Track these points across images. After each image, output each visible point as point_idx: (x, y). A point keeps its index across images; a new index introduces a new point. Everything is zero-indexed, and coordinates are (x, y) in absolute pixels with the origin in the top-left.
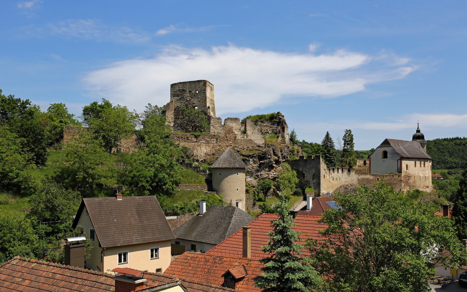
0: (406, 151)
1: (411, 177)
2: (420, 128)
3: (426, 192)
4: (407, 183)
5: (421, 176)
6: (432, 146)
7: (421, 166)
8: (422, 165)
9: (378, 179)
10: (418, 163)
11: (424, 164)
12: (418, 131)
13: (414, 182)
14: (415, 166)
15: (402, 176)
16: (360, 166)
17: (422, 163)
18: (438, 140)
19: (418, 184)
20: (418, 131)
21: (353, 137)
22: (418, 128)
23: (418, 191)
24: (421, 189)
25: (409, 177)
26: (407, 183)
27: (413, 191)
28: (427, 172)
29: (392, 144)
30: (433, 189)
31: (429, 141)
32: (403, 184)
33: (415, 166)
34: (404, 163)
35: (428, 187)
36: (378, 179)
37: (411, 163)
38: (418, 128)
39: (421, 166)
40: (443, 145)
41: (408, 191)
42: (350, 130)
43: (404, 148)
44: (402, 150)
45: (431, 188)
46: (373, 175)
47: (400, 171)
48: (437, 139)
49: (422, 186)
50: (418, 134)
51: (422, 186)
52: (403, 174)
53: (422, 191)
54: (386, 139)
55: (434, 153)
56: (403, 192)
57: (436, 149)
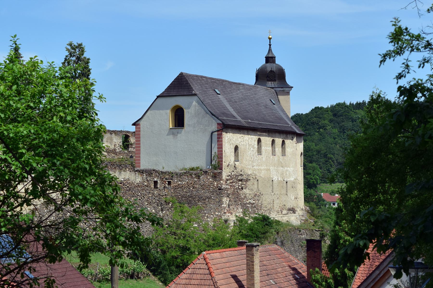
0: (235, 109)
1: (247, 180)
2: (275, 52)
3: (288, 224)
4: (237, 199)
5: (275, 178)
6: (326, 122)
7: (274, 153)
8: (278, 149)
9: (156, 183)
10: (266, 140)
11: (283, 143)
12: (270, 59)
13: (257, 196)
14: (259, 151)
15: (224, 175)
16: (114, 151)
17: (279, 141)
18: (339, 103)
19: (266, 200)
20: (270, 59)
21: (91, 66)
22: (270, 50)
23: (265, 221)
24: (274, 216)
25: (241, 179)
26: (237, 199)
27: (255, 219)
28: (291, 169)
29: (196, 89)
30: (307, 216)
31: (322, 108)
32: (226, 200)
33: (259, 151)
34: (230, 139)
35: (293, 210)
36: (156, 183)
37: (247, 141)
38: (270, 50)
39: (274, 153)
40: (353, 120)
41: (241, 220)
42: (80, 45)
43: (229, 101)
44: (225, 107)
45: (301, 213)
46: (141, 172)
47: (217, 166)
48: (338, 105)
49: (277, 207)
50: (270, 67)
51: (277, 207)
52: (225, 174)
53: (278, 222)
54: (181, 75)
55: (331, 140)
56: (226, 221)
57: (336, 131)
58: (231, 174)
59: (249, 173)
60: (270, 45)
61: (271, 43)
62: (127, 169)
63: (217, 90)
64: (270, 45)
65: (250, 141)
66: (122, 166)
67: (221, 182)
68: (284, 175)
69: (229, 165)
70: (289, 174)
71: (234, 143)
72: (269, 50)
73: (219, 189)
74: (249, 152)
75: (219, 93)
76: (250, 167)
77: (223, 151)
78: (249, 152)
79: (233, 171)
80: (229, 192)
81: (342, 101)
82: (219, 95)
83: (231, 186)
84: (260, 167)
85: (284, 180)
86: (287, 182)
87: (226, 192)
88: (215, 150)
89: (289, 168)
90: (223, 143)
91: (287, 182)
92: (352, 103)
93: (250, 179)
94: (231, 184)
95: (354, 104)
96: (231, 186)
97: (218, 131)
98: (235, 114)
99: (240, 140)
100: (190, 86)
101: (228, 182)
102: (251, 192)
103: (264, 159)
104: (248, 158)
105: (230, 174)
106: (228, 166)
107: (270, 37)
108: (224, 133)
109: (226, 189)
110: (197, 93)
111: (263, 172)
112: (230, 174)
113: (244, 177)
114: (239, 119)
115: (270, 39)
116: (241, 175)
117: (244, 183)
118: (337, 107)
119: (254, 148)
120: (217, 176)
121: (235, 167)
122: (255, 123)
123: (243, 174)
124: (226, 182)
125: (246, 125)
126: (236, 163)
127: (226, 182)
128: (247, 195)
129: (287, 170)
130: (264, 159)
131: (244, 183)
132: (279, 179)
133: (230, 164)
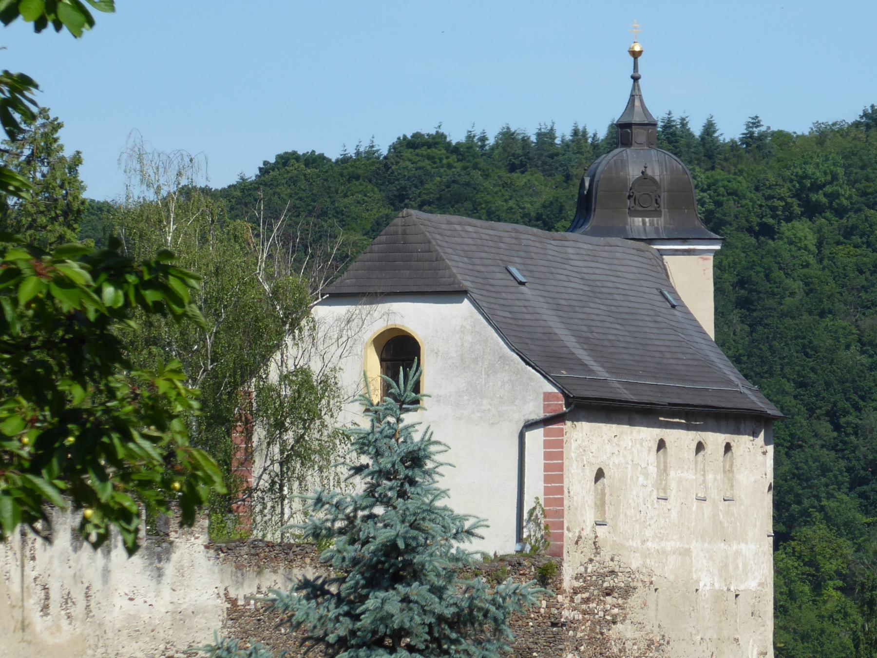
31: (314, 160)
48: (413, 144)
58: (586, 568)
59: (634, 567)
60: (636, 79)
61: (641, 72)
62: (308, 560)
63: (514, 270)
64: (636, 79)
65: (635, 451)
66: (294, 549)
67: (560, 598)
68: (731, 568)
69: (580, 537)
70: (745, 565)
71: (593, 460)
72: (632, 97)
73: (554, 625)
74: (634, 493)
75: (523, 280)
76: (635, 544)
77: (566, 491)
78: (634, 493)
79: (591, 560)
80: (579, 635)
81: (428, 129)
82: (523, 288)
83: (584, 613)
84: (663, 544)
85: (729, 590)
86: (737, 596)
87: (571, 633)
88: (535, 489)
89: (743, 546)
90: (566, 463)
91: (737, 596)
92: (478, 133)
93: (635, 588)
94: (584, 607)
95: (491, 141)
96: (584, 613)
97: (546, 422)
98: (581, 354)
99: (609, 448)
100: (439, 259)
101: (578, 598)
102: (637, 635)
103: (674, 514)
104: (631, 512)
105: (582, 569)
106: (577, 543)
107: (637, 48)
108: (754, 461)
109: (571, 624)
110: (467, 285)
111: (672, 559)
112: (582, 569)
113: (620, 581)
114: (602, 373)
115: (635, 55)
116: (613, 572)
117: (620, 601)
118: (408, 153)
119: (647, 476)
120: (547, 576)
121: (594, 543)
122: (676, 391)
123: (617, 570)
124: (572, 600)
125: (626, 395)
126: (601, 531)
127: (572, 600)
128: (628, 645)
129: (738, 553)
130: (674, 514)
131: (620, 601)
132: (717, 586)
133: (584, 534)
